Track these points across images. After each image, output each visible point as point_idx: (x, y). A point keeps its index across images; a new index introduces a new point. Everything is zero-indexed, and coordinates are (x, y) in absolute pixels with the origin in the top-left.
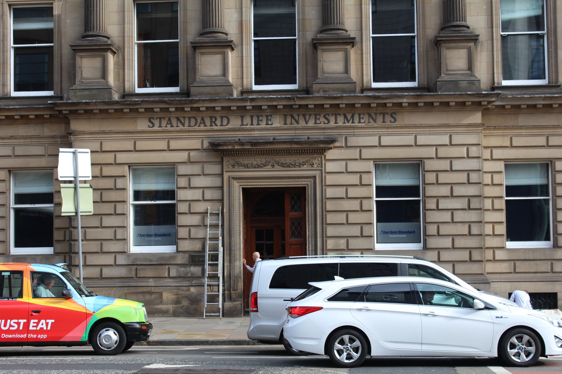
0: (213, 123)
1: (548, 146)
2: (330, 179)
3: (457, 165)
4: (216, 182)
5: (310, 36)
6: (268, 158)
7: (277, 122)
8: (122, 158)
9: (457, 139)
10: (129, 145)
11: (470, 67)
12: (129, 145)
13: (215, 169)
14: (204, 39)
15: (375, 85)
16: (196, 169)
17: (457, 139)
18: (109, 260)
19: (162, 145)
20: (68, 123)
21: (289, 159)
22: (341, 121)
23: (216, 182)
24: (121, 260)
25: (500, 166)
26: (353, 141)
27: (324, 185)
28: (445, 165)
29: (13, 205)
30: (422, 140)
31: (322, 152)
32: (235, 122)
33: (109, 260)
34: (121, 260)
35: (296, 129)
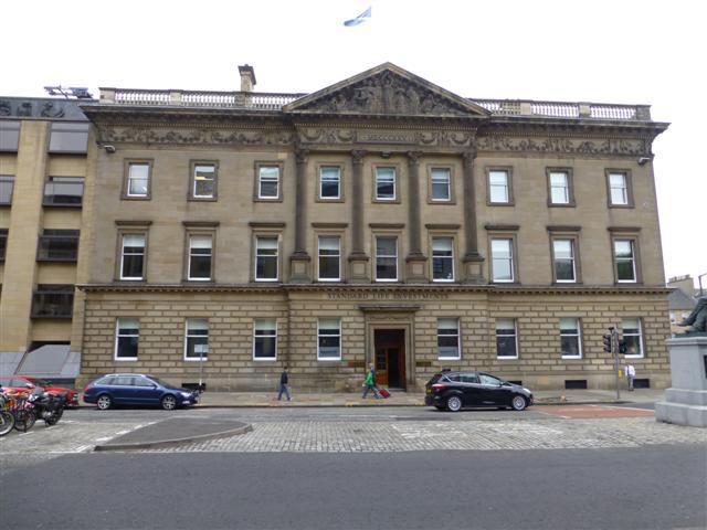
1: (338, 309)
2: (417, 326)
3: (597, 320)
4: (362, 326)
5: (405, 255)
6: (388, 315)
7: (391, 297)
8: (315, 313)
9: (476, 307)
10: (254, 308)
11: (481, 274)
12: (254, 308)
13: (362, 319)
14: (355, 256)
15: (378, 280)
16: (352, 319)
17: (476, 307)
18: (307, 364)
19: (335, 307)
20: (287, 295)
21: (397, 316)
22: (422, 297)
23: (362, 326)
24: (314, 364)
25: (435, 319)
26: (427, 308)
27: (414, 329)
28: (591, 320)
29: (117, 335)
30: (460, 307)
31: (413, 312)
32: (371, 297)
33: (307, 364)
34: (314, 364)
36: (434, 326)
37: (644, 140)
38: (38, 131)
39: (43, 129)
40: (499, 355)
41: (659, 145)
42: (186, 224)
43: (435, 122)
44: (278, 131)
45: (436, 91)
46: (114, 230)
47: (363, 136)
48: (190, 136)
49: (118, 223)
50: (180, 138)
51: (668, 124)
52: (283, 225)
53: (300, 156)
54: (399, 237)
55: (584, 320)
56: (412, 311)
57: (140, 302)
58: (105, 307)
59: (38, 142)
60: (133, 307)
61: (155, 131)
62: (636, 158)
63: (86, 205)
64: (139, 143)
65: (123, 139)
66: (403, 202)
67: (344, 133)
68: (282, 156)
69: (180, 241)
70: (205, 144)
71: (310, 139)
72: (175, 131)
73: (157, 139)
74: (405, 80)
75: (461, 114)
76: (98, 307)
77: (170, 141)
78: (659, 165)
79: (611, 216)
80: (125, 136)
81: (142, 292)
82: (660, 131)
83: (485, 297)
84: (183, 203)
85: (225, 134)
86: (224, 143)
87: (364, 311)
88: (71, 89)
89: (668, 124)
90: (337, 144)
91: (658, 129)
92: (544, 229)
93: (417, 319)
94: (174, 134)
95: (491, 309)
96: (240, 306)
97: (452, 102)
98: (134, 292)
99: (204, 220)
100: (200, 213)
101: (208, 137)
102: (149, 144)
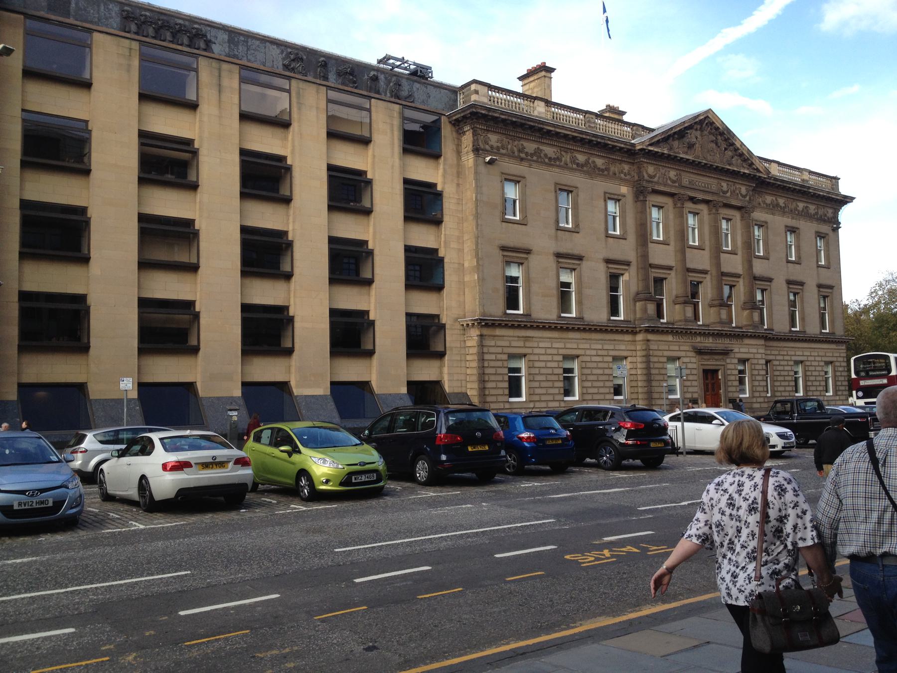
0: (692, 339)
7: (711, 340)
19: (676, 348)
21: (716, 357)
35: (717, 343)
36: (561, 365)
37: (835, 209)
38: (392, 117)
39: (396, 115)
40: (510, 396)
41: (845, 214)
42: (558, 255)
43: (735, 174)
44: (621, 161)
45: (738, 145)
46: (498, 255)
47: (686, 179)
48: (553, 156)
49: (504, 249)
50: (546, 155)
51: (854, 198)
52: (628, 264)
53: (641, 193)
54: (738, 286)
55: (808, 363)
56: (726, 353)
57: (527, 338)
58: (500, 343)
59: (392, 131)
60: (521, 344)
61: (526, 144)
62: (831, 225)
63: (15, 144)
64: (511, 155)
65: (498, 148)
66: (740, 253)
67: (672, 174)
68: (624, 190)
69: (553, 273)
70: (565, 167)
71: (650, 176)
72: (541, 147)
73: (527, 154)
74: (717, 129)
75: (753, 173)
76: (493, 343)
77: (537, 158)
78: (843, 233)
79: (818, 274)
80: (499, 145)
81: (525, 327)
82: (845, 203)
83: (762, 342)
84: (552, 231)
85: (581, 158)
86: (580, 167)
87: (700, 352)
88: (415, 64)
89: (854, 198)
90: (669, 185)
91: (847, 200)
92: (785, 282)
93: (728, 361)
94: (541, 150)
95: (769, 352)
96: (602, 344)
97: (744, 155)
98: (519, 327)
99: (570, 252)
100: (566, 247)
101: (567, 158)
102: (522, 159)
